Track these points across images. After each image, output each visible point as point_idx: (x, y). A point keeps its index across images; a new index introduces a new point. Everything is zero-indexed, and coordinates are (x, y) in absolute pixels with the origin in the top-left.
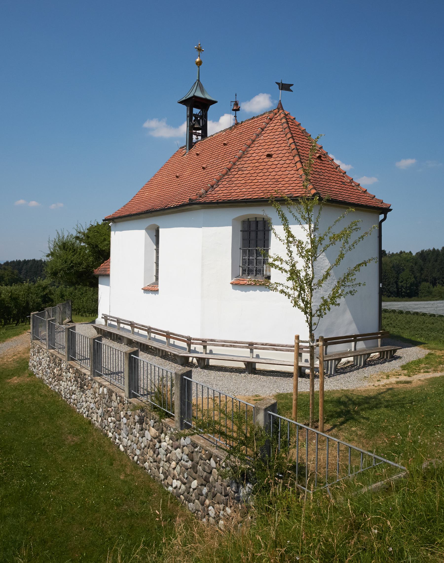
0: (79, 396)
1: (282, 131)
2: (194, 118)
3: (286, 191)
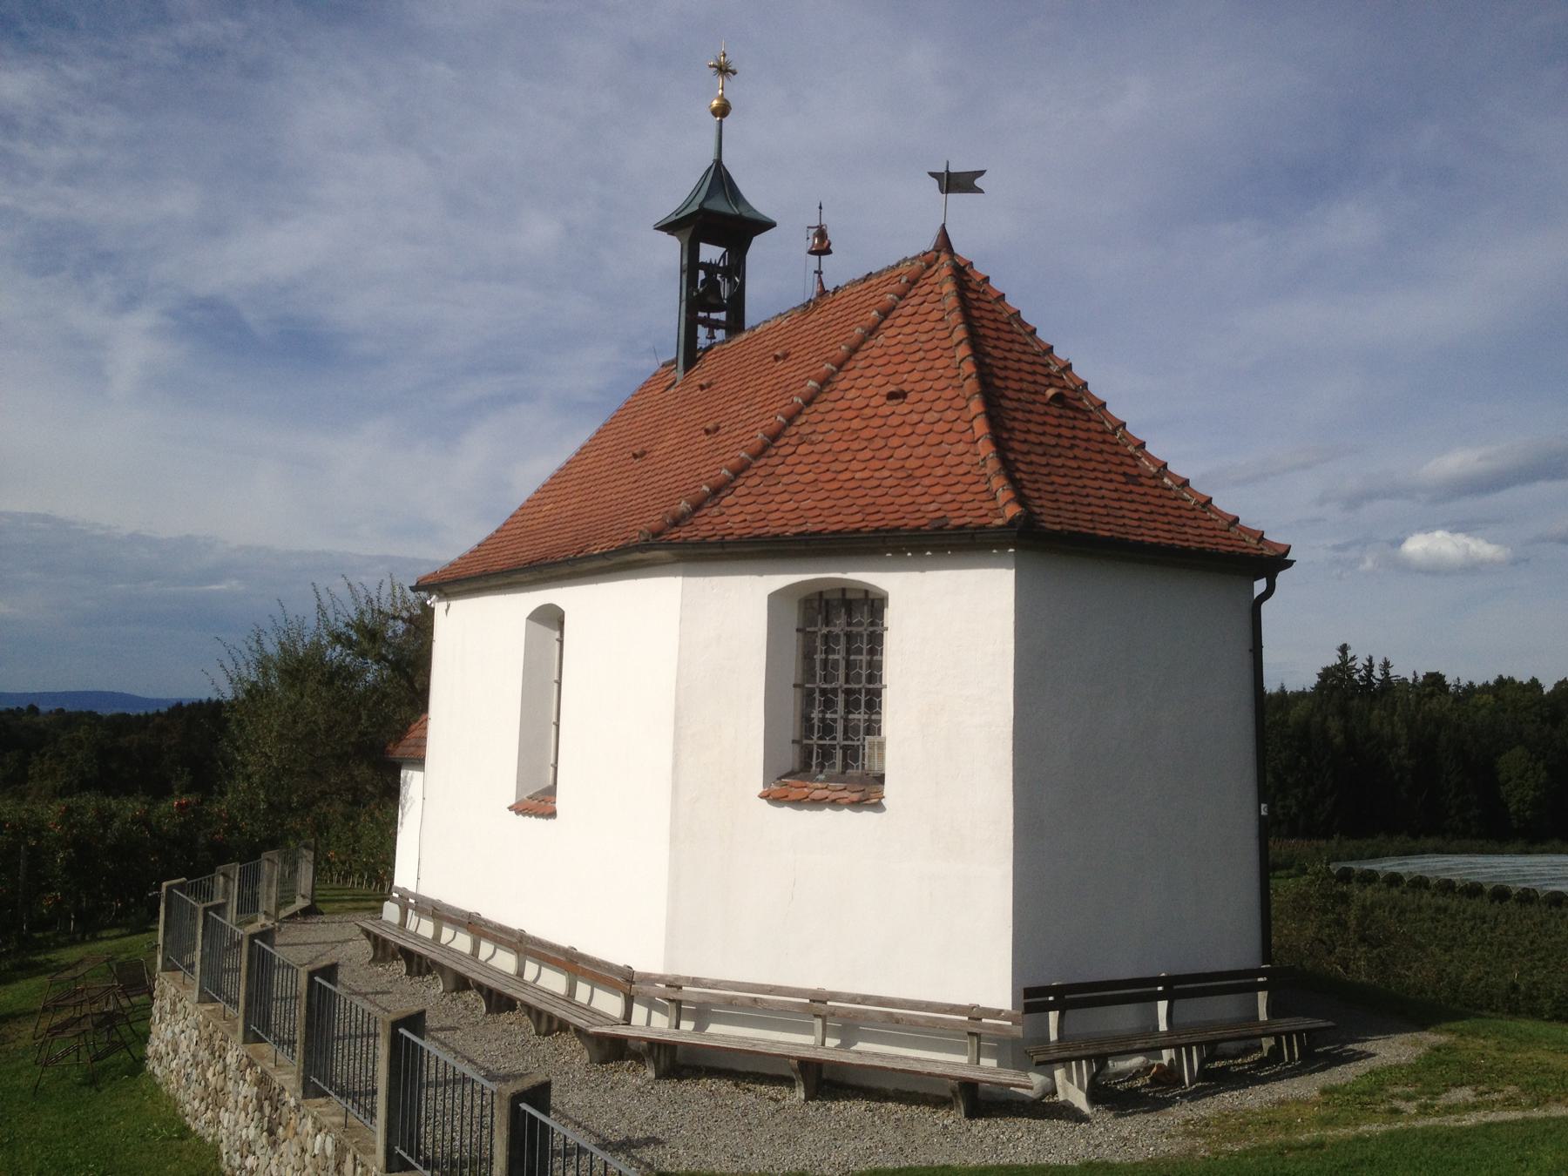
0: (263, 1161)
1: (942, 320)
2: (702, 275)
3: (932, 507)
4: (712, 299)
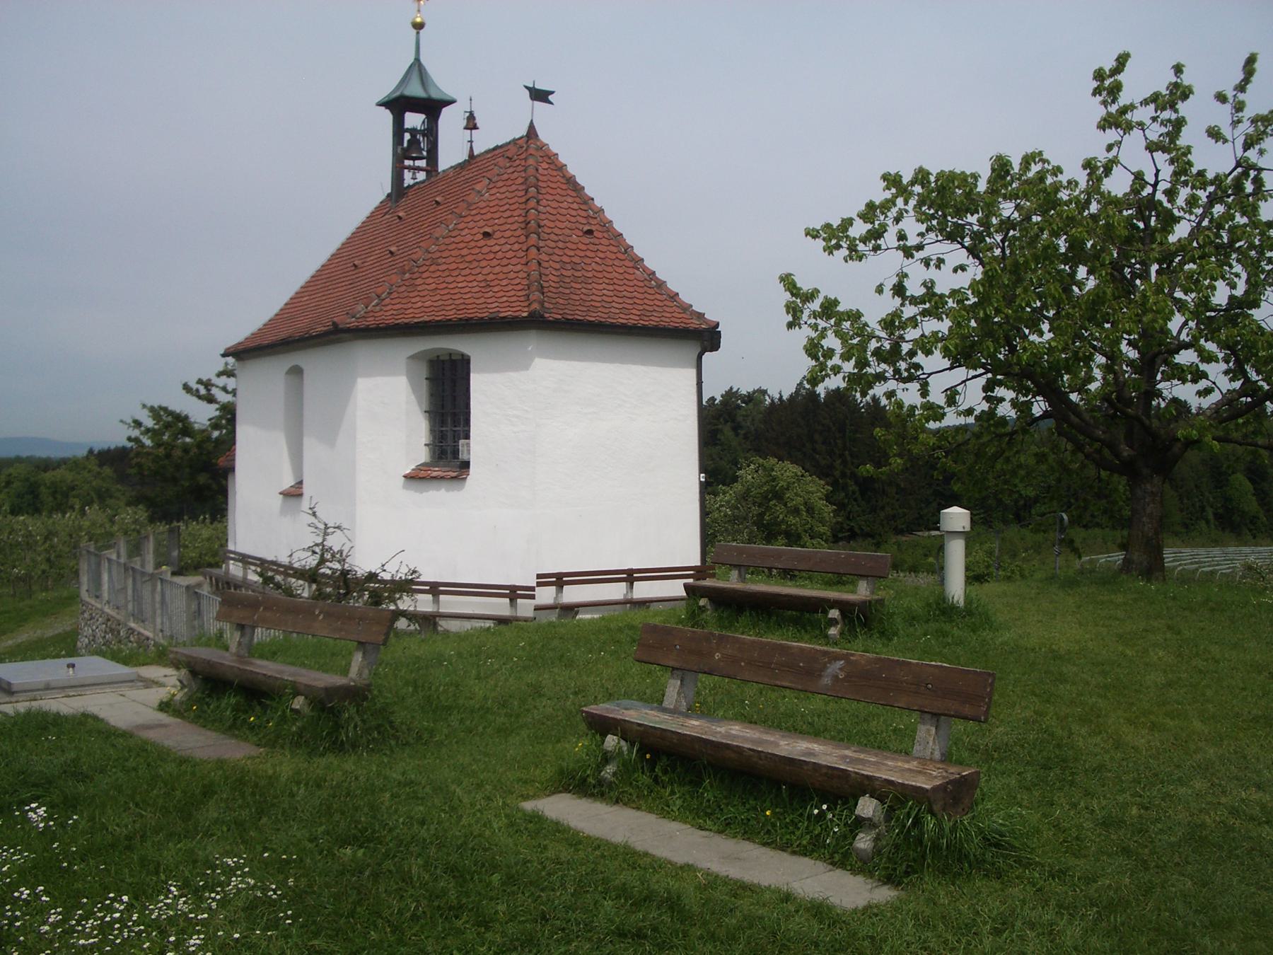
4: (413, 147)
